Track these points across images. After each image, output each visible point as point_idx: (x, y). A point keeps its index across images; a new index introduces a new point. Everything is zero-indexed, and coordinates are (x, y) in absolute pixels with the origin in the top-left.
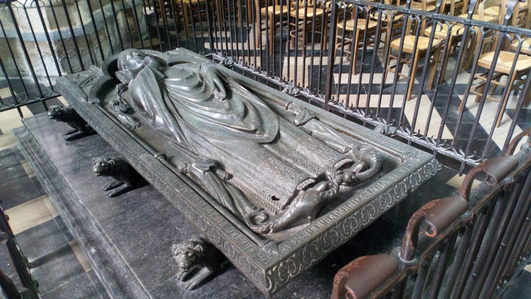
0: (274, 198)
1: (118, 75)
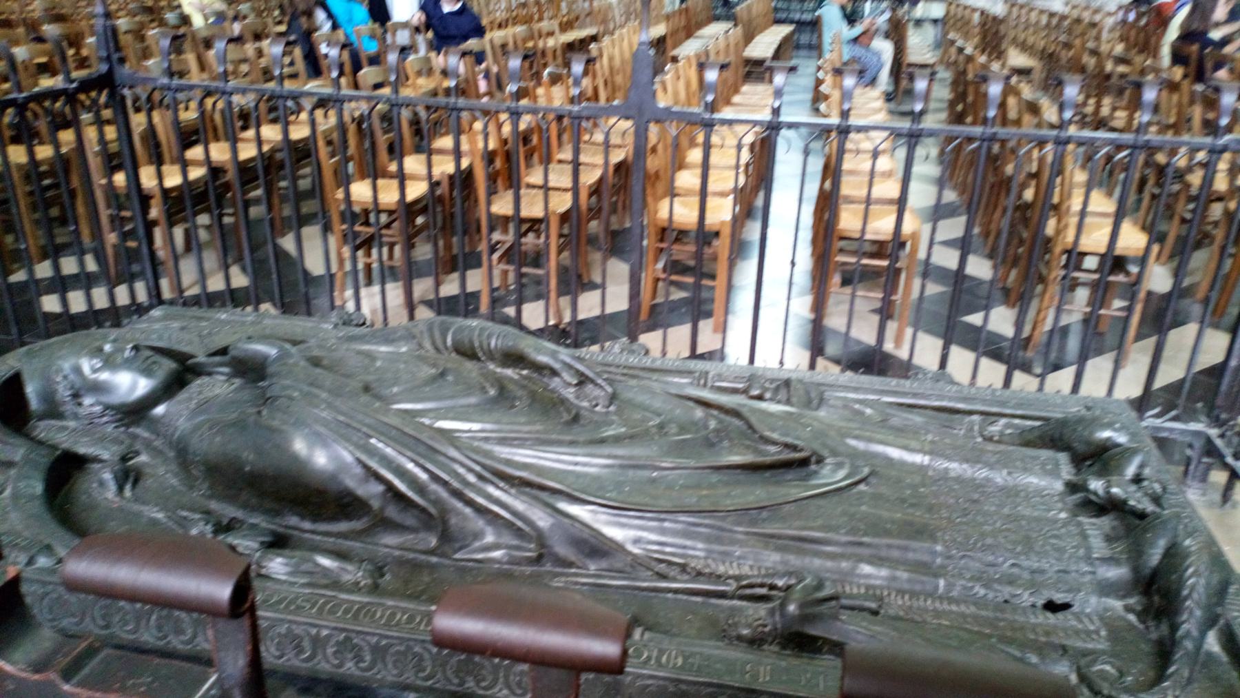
0: (1051, 607)
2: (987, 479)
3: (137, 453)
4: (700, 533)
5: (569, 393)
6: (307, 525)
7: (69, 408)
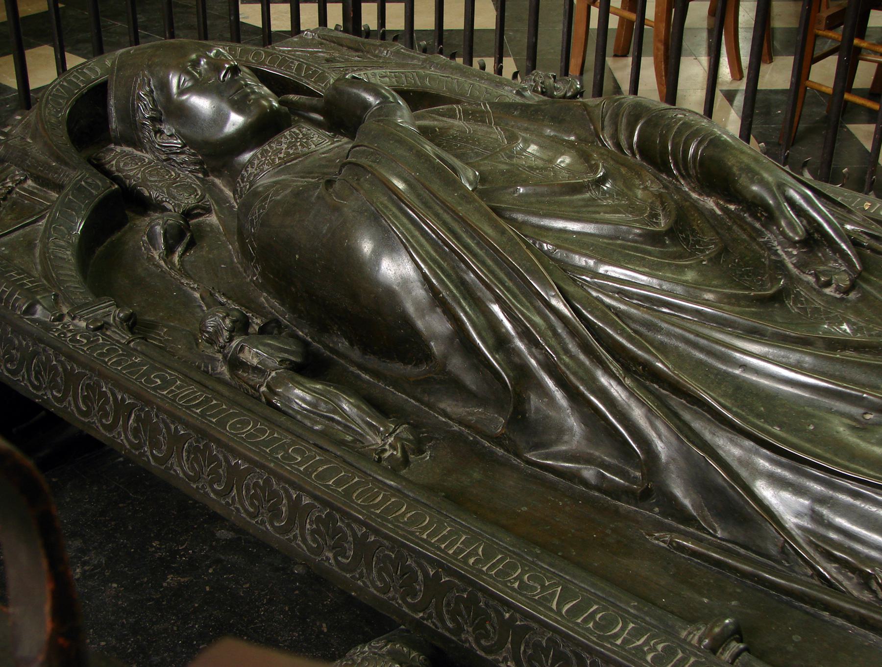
1: (123, 160)
2: (694, 190)
3: (208, 211)
5: (789, 258)
6: (356, 354)
7: (148, 133)
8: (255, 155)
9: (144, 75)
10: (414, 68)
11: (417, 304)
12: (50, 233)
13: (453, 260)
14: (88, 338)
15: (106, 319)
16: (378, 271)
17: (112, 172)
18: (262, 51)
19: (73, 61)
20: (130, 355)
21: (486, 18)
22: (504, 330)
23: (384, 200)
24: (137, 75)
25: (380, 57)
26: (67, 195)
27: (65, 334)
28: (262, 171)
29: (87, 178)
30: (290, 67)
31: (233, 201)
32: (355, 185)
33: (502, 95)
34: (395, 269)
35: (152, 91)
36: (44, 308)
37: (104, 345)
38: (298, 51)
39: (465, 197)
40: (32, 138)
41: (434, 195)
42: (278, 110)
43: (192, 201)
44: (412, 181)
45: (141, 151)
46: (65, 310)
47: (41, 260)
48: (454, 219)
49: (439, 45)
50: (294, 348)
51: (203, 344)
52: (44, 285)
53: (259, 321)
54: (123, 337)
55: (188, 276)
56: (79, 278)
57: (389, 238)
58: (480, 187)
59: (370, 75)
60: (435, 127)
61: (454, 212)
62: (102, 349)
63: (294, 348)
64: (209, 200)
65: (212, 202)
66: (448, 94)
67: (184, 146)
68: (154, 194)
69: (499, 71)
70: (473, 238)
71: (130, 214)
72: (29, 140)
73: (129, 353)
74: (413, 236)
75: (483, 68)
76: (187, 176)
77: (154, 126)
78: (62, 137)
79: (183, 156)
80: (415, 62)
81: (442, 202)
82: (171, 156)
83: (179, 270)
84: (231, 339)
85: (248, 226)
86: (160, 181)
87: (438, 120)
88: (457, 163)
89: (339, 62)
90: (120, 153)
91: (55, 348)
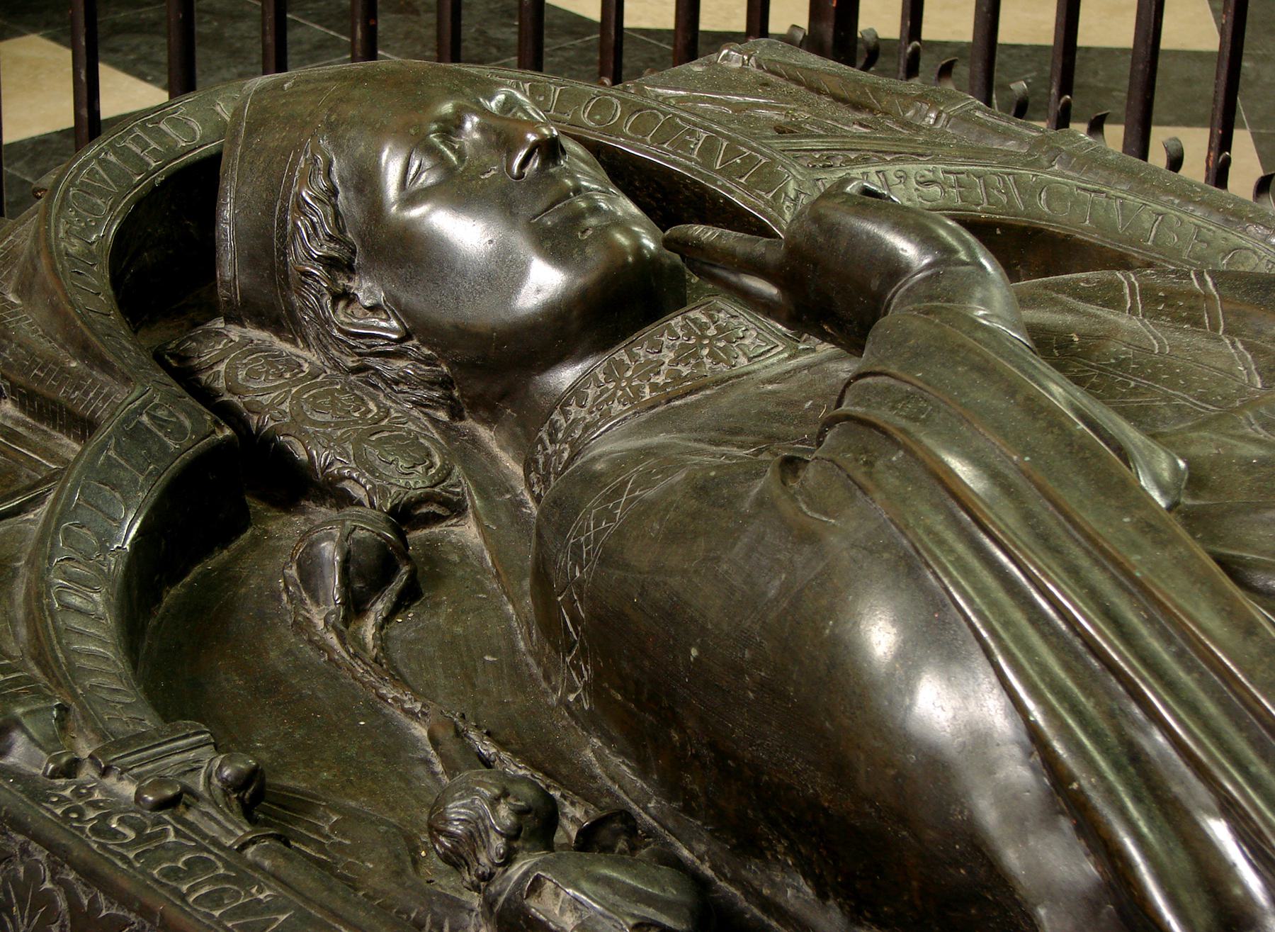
1: (236, 355)
3: (456, 509)
4: (1034, 605)
7: (312, 299)
8: (587, 376)
9: (317, 147)
10: (1006, 164)
11: (1007, 797)
12: (54, 545)
13: (1109, 692)
14: (139, 829)
15: (187, 781)
16: (910, 708)
17: (217, 394)
18: (614, 95)
19: (123, 94)
20: (243, 880)
21: (1192, 27)
22: (1237, 891)
23: (938, 522)
24: (298, 148)
25: (919, 128)
26: (103, 447)
27: (81, 813)
28: (606, 416)
29: (157, 407)
30: (684, 145)
31: (521, 487)
32: (859, 475)
33: (1238, 248)
34: (953, 707)
35: (333, 192)
36: (31, 739)
37: (178, 849)
38: (703, 100)
39: (1151, 527)
40: (17, 292)
41: (1069, 518)
42: (654, 261)
43: (417, 483)
44: (1012, 476)
45: (293, 342)
46: (85, 751)
47: (29, 613)
48: (1120, 585)
49: (1061, 95)
50: (672, 893)
51: (432, 862)
52: (31, 679)
53: (578, 813)
54: (226, 828)
55: (399, 680)
56: (122, 666)
57: (943, 624)
58: (1187, 501)
59: (892, 179)
60: (1070, 329)
61: (1118, 565)
62: (175, 859)
63: (672, 893)
64: (462, 483)
65: (467, 485)
66: (1095, 238)
67: (407, 336)
68: (321, 456)
69: (1219, 175)
70: (1167, 639)
71: (255, 505)
72: (12, 298)
73: (243, 875)
74: (1007, 624)
75: (1175, 162)
76: (406, 413)
77: (333, 281)
78: (95, 293)
79: (401, 363)
80: (1011, 145)
81: (1088, 537)
82: (372, 361)
83: (376, 660)
84: (508, 859)
85: (565, 560)
86: (338, 426)
87: (1071, 310)
88: (1132, 435)
89: (810, 135)
90: (240, 345)
91: (49, 845)
